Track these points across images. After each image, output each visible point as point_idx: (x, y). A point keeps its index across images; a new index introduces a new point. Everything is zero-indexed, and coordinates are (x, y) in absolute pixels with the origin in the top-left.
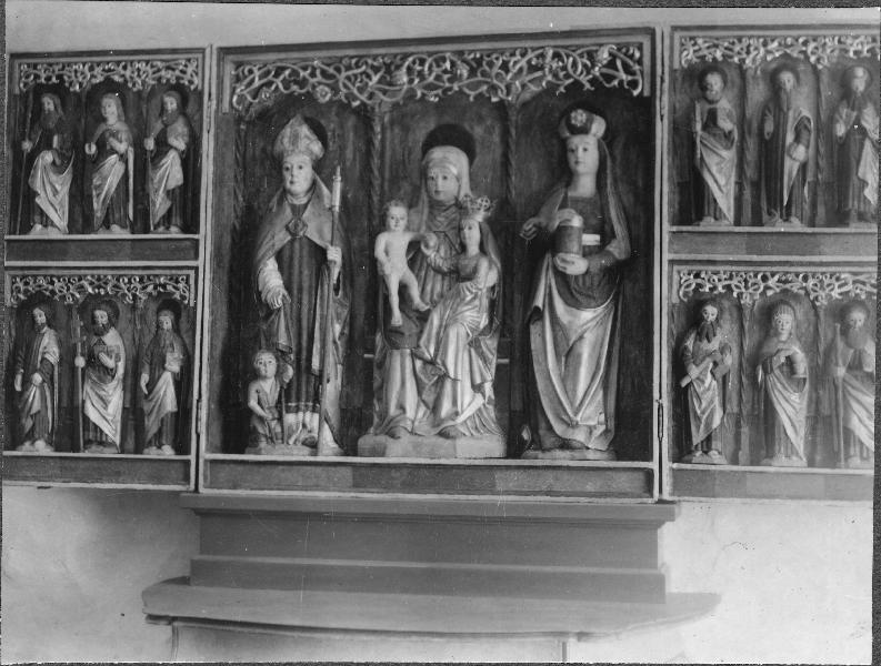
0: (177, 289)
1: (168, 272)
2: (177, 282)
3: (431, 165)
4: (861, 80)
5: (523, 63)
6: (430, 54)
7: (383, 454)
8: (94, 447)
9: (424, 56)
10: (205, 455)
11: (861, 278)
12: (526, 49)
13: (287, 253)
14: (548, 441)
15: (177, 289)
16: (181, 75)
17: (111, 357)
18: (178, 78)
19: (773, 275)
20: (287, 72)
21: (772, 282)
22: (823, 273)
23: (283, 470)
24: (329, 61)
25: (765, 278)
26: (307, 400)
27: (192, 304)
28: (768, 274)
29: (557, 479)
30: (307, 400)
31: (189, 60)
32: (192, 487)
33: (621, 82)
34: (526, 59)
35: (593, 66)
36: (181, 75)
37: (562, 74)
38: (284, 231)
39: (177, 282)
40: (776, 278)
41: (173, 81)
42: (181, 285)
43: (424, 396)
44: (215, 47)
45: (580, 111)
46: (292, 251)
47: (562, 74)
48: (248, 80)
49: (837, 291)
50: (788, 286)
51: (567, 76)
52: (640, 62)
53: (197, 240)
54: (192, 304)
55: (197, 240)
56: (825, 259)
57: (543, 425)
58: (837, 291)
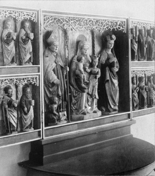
0: (33, 81)
1: (31, 76)
2: (33, 79)
3: (85, 46)
4: (152, 31)
5: (105, 23)
6: (88, 19)
7: (83, 119)
8: (13, 133)
9: (87, 19)
10: (44, 128)
11: (28, 14)
12: (106, 20)
13: (56, 69)
14: (111, 110)
15: (33, 81)
16: (31, 17)
17: (17, 104)
18: (30, 18)
19: (7, 11)
20: (57, 19)
21: (7, 13)
22: (20, 12)
23: (62, 128)
24: (67, 18)
25: (5, 12)
26: (65, 108)
27: (38, 85)
28: (6, 11)
29: (114, 118)
30: (65, 108)
31: (33, 13)
32: (42, 138)
33: (121, 29)
34: (105, 22)
35: (117, 25)
36: (31, 17)
37: (111, 26)
38: (54, 63)
39: (33, 79)
40: (9, 12)
41: (29, 19)
42: (34, 80)
43: (89, 104)
44: (41, 10)
45: (114, 35)
46: (57, 69)
47: (111, 26)
48: (48, 20)
49: (23, 17)
50: (11, 15)
51: (113, 27)
52: (124, 25)
53: (39, 67)
54: (38, 85)
55: (39, 67)
56: (151, 67)
57: (109, 107)
58: (23, 17)
